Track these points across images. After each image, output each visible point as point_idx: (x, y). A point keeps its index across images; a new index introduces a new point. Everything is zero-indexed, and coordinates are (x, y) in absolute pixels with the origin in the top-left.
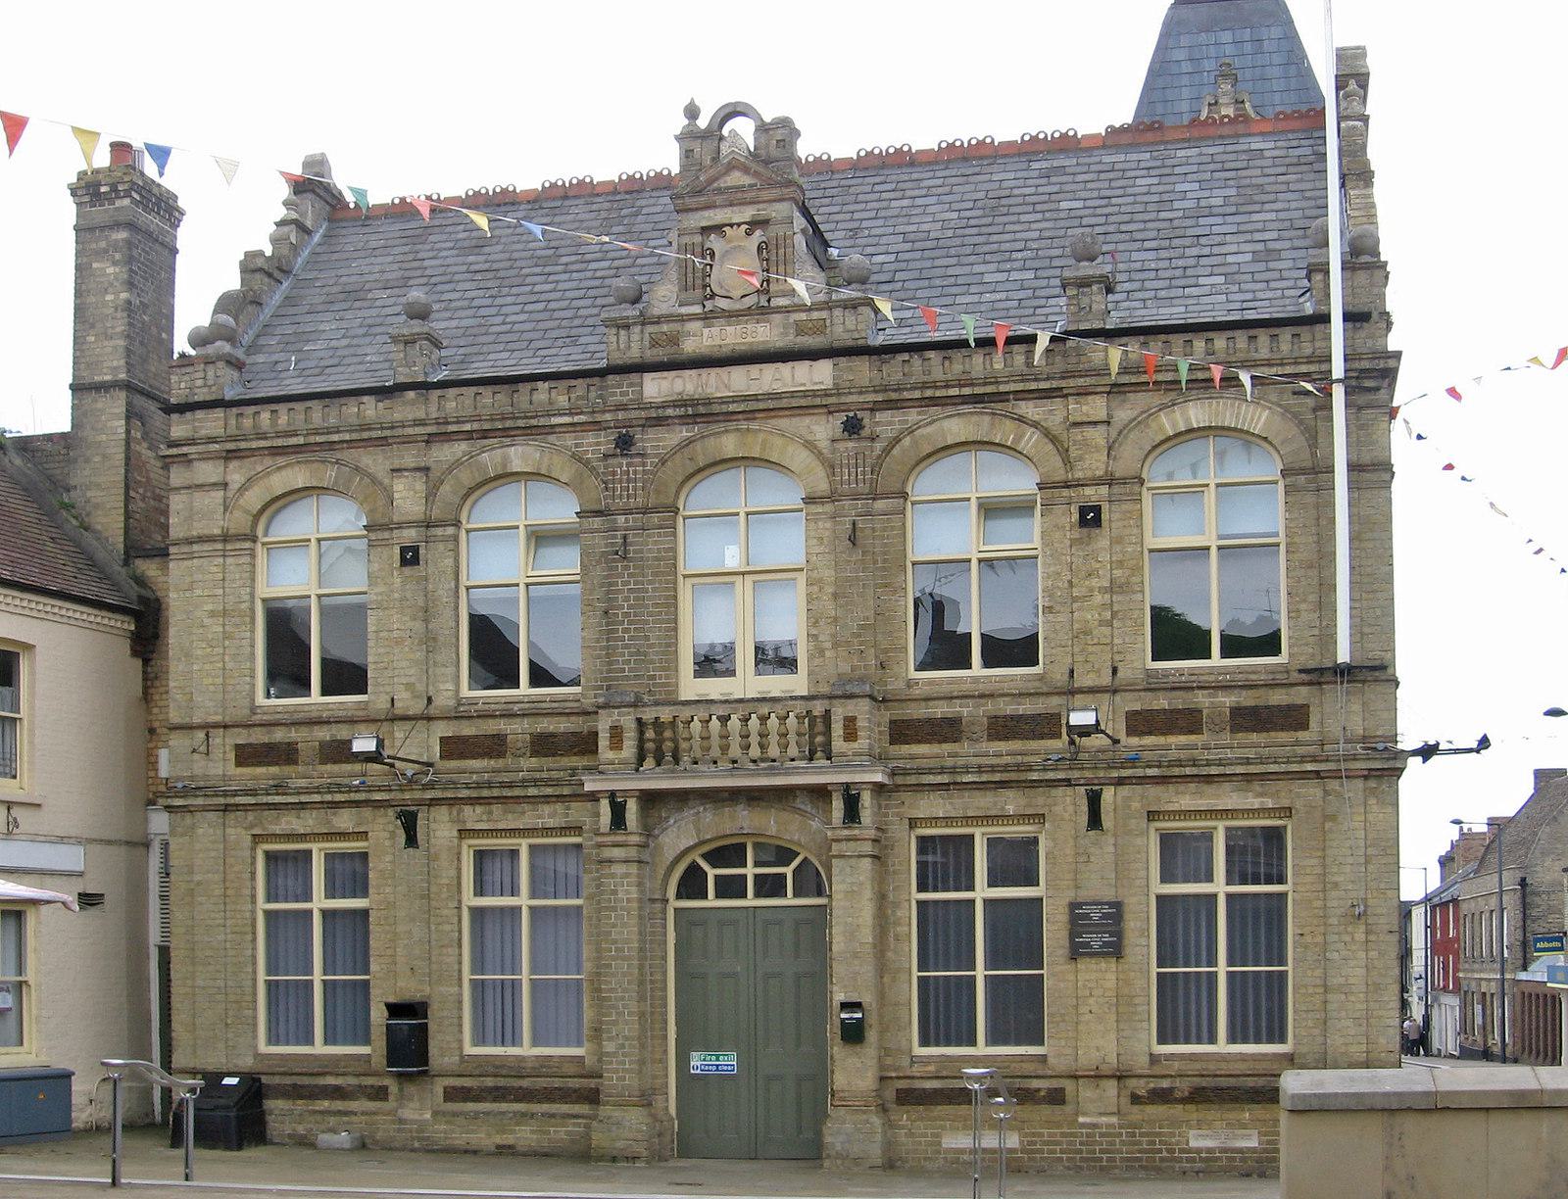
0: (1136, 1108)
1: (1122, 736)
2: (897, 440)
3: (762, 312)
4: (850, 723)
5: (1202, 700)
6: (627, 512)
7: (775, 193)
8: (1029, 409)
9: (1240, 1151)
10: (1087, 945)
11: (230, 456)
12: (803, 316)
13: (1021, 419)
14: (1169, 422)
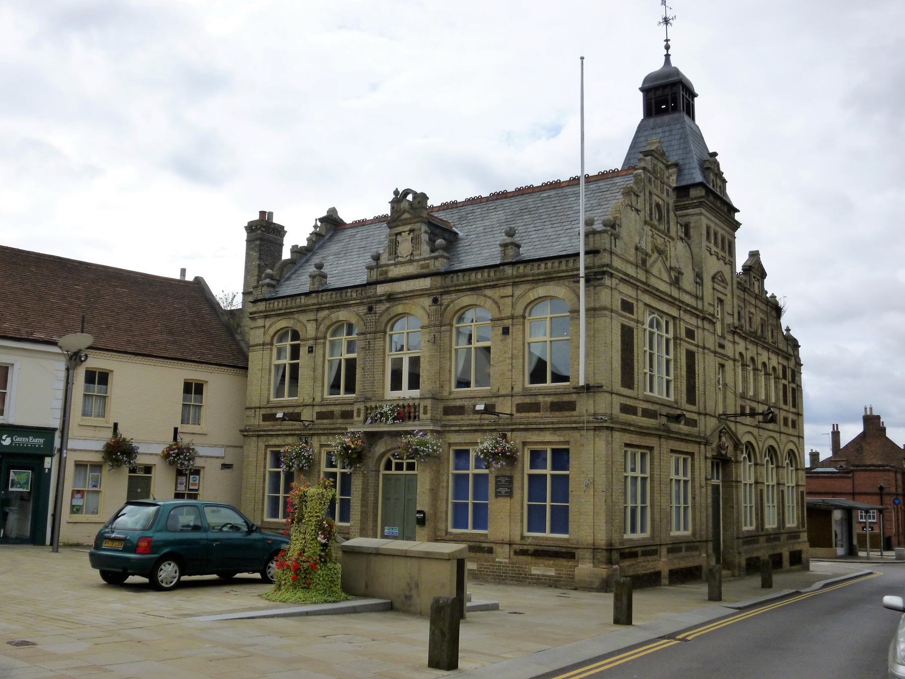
0: (515, 557)
1: (514, 412)
2: (448, 305)
3: (411, 261)
4: (425, 407)
5: (540, 399)
6: (370, 333)
7: (416, 220)
8: (488, 292)
9: (548, 576)
10: (500, 492)
11: (266, 317)
12: (423, 262)
13: (485, 296)
14: (533, 295)
